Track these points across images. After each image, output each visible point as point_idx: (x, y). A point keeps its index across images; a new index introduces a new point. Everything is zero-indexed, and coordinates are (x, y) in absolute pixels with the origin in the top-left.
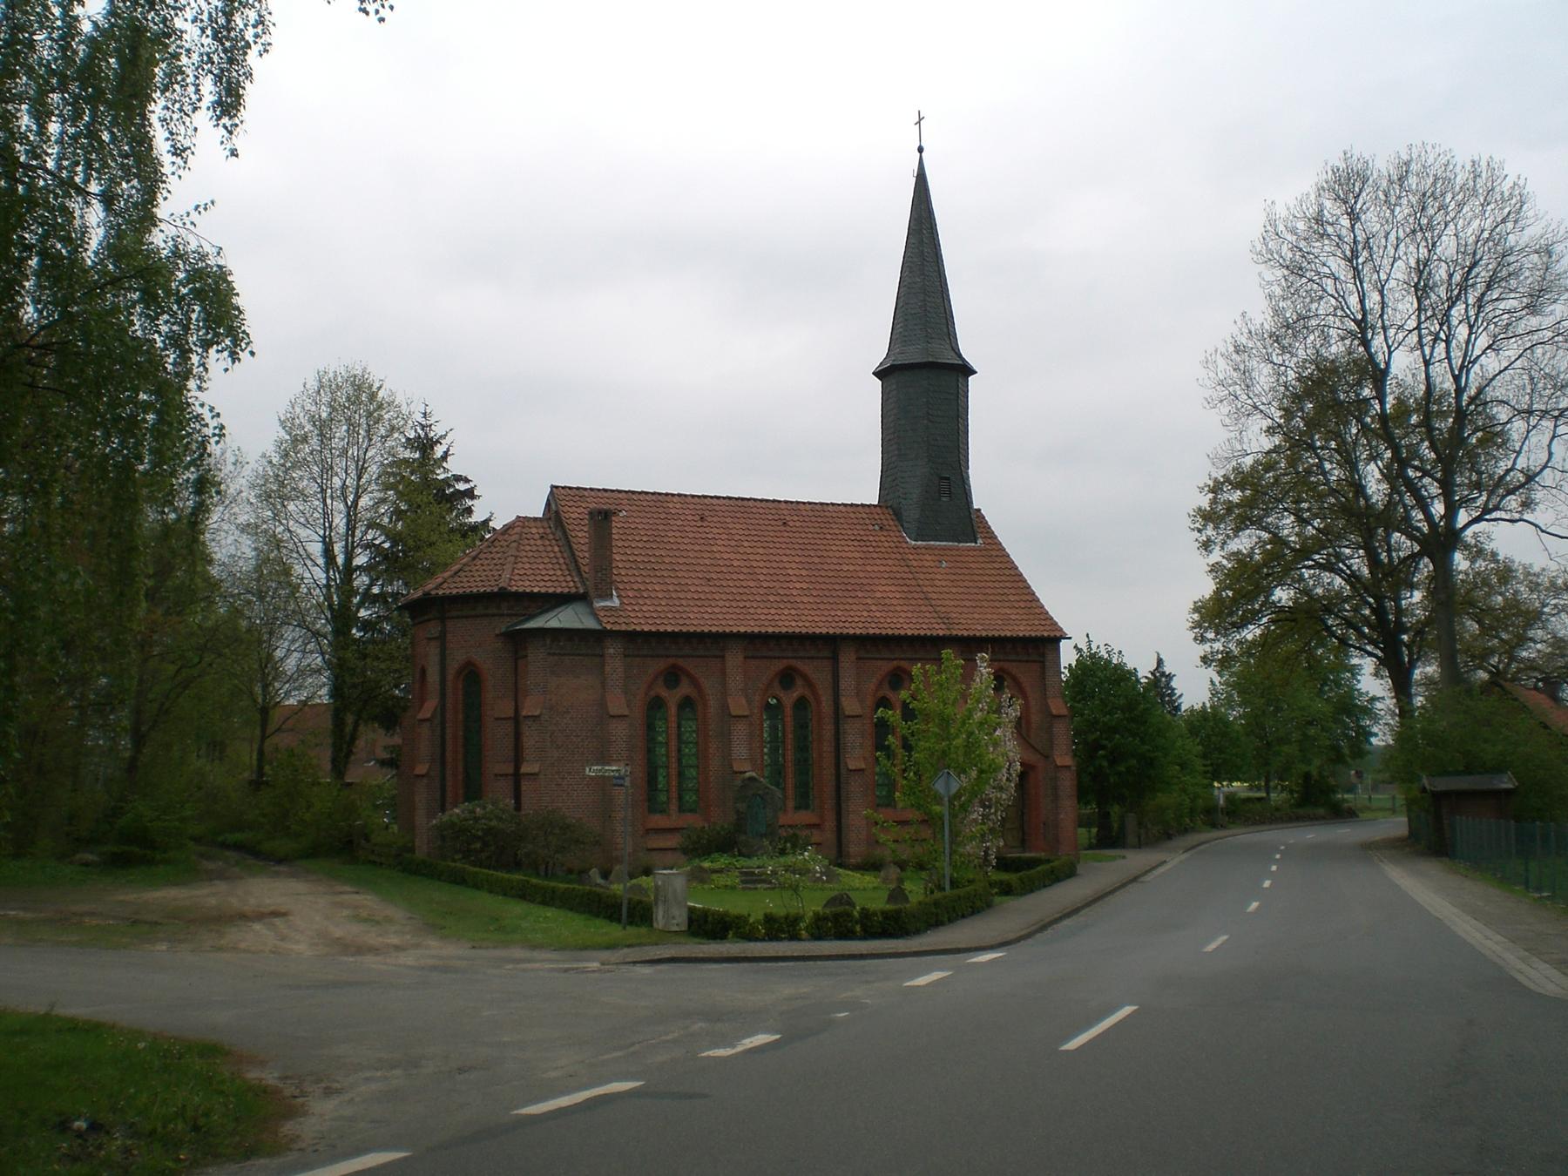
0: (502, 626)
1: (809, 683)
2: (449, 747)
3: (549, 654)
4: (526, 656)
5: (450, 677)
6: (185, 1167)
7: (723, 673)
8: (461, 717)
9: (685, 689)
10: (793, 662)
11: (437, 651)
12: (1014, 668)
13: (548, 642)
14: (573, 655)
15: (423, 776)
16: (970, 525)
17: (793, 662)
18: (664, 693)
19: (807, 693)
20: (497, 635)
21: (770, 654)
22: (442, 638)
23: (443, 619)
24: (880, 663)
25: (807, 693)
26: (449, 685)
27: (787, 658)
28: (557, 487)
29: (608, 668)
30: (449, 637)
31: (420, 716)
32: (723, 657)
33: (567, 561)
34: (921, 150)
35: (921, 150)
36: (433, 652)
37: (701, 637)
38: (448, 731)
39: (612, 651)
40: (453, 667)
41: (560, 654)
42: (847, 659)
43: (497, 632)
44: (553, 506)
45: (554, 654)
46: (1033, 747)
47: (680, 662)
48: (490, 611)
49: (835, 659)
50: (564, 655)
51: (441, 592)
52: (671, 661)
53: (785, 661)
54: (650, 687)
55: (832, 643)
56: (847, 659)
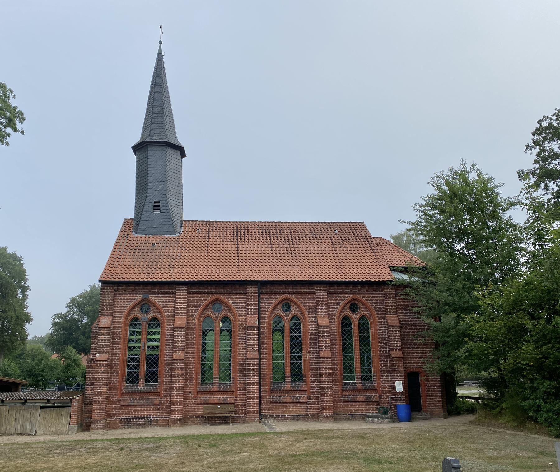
34: (161, 43)
35: (161, 43)
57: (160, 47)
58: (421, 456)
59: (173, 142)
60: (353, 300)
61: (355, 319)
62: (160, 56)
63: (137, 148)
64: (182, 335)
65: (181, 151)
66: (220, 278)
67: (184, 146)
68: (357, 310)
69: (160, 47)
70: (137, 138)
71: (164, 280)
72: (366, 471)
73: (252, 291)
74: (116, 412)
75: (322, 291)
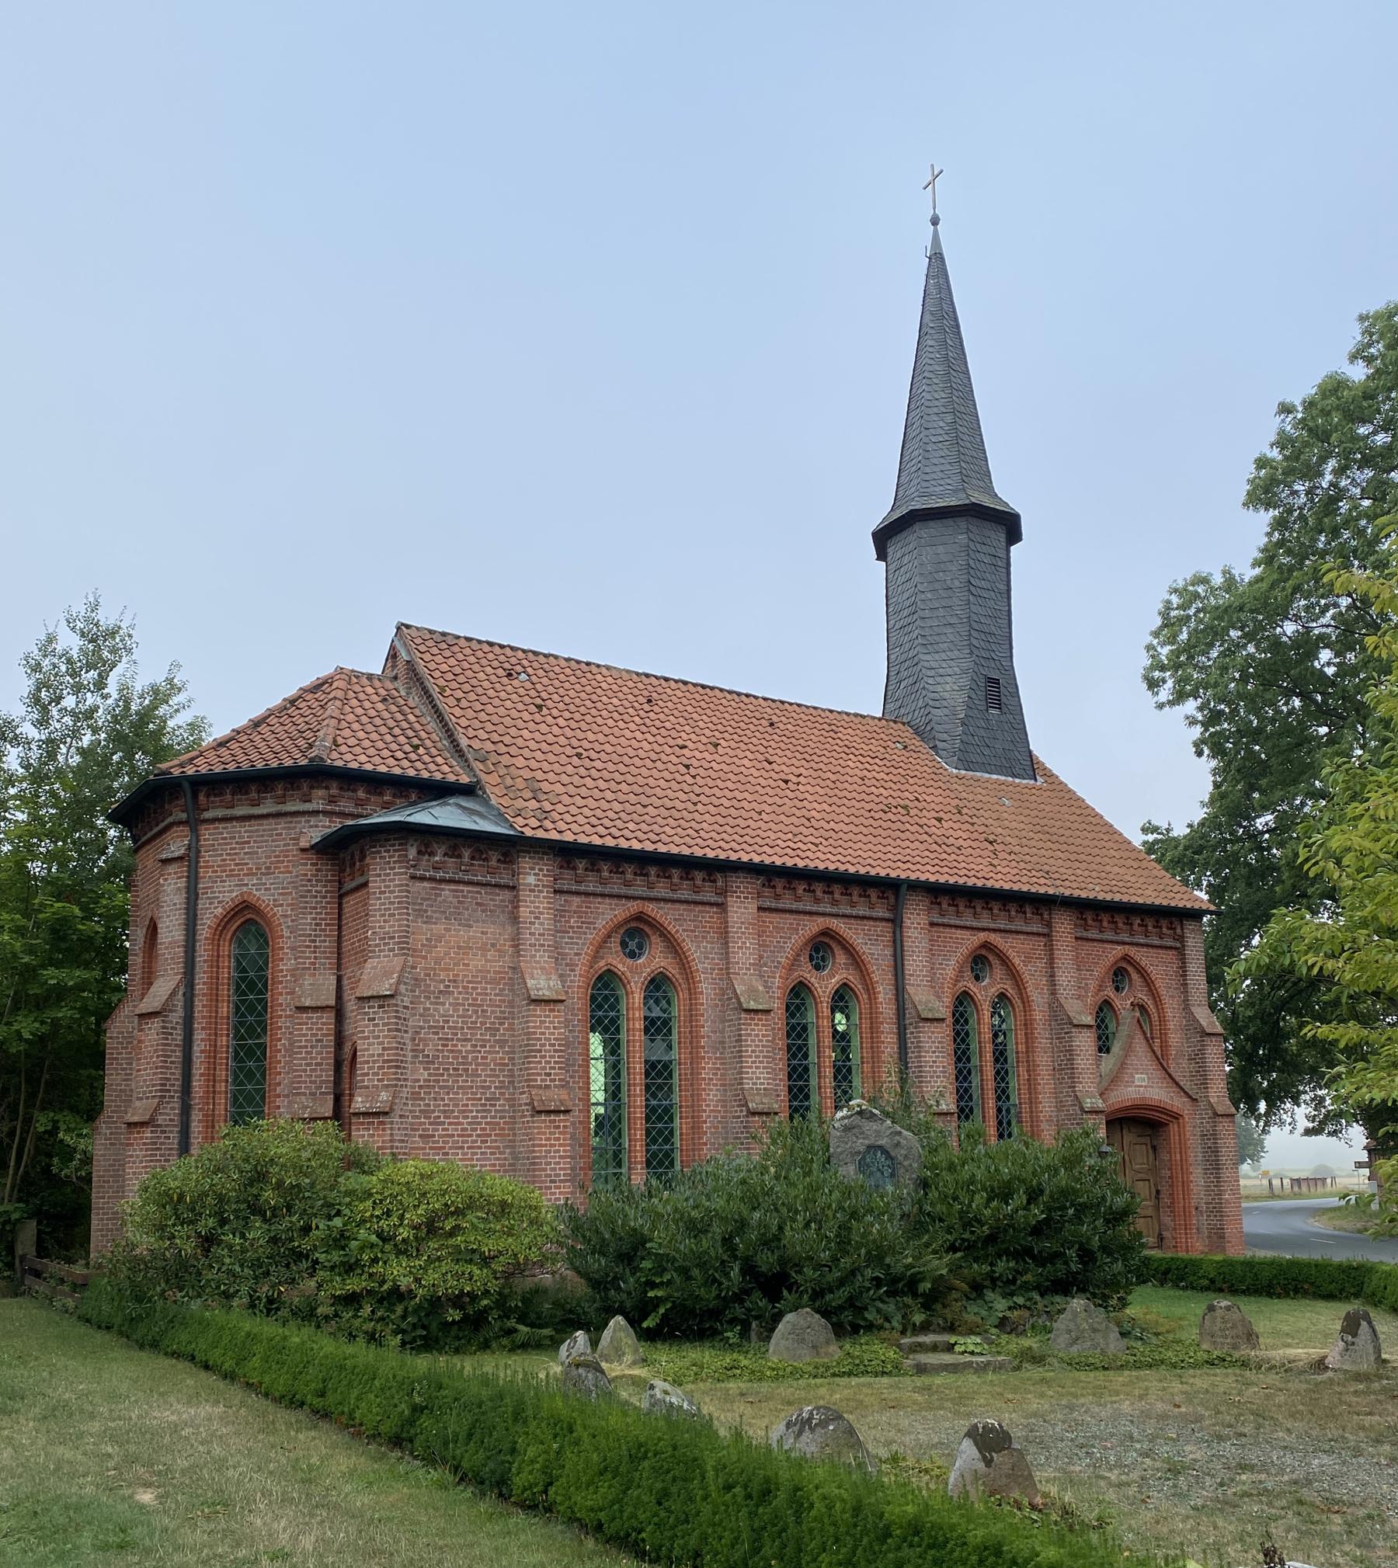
0: (315, 832)
1: (856, 961)
2: (199, 1068)
3: (413, 877)
4: (365, 885)
5: (204, 932)
6: (915, 1402)
7: (724, 934)
8: (224, 1009)
9: (655, 960)
10: (835, 924)
11: (182, 883)
12: (1142, 957)
13: (412, 852)
14: (459, 882)
15: (143, 1124)
16: (1031, 767)
17: (835, 924)
18: (621, 964)
19: (854, 979)
20: (303, 850)
21: (800, 906)
22: (191, 860)
23: (194, 824)
24: (959, 933)
25: (854, 979)
26: (203, 953)
27: (823, 914)
28: (408, 627)
29: (524, 912)
30: (206, 856)
31: (145, 1006)
32: (722, 906)
33: (434, 737)
34: (935, 221)
35: (935, 221)
36: (172, 888)
37: (688, 865)
38: (199, 1035)
39: (531, 880)
40: (210, 913)
41: (432, 879)
42: (916, 918)
43: (304, 844)
44: (404, 655)
45: (422, 879)
46: (1177, 1084)
47: (650, 908)
48: (290, 807)
49: (896, 922)
50: (442, 881)
51: (190, 771)
52: (634, 907)
53: (820, 920)
54: (596, 956)
55: (891, 890)
56: (916, 918)
57: (936, 237)
58: (1220, 1524)
59: (987, 502)
60: (1139, 972)
61: (636, 974)
62: (937, 259)
63: (884, 538)
64: (394, 943)
65: (1009, 526)
66: (838, 864)
67: (1018, 510)
68: (640, 954)
69: (936, 237)
70: (880, 509)
71: (708, 856)
72: (1396, 1554)
73: (533, 876)
74: (449, 1075)
75: (1064, 926)
